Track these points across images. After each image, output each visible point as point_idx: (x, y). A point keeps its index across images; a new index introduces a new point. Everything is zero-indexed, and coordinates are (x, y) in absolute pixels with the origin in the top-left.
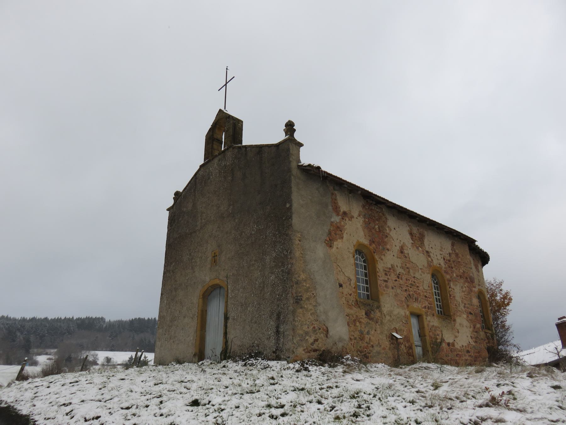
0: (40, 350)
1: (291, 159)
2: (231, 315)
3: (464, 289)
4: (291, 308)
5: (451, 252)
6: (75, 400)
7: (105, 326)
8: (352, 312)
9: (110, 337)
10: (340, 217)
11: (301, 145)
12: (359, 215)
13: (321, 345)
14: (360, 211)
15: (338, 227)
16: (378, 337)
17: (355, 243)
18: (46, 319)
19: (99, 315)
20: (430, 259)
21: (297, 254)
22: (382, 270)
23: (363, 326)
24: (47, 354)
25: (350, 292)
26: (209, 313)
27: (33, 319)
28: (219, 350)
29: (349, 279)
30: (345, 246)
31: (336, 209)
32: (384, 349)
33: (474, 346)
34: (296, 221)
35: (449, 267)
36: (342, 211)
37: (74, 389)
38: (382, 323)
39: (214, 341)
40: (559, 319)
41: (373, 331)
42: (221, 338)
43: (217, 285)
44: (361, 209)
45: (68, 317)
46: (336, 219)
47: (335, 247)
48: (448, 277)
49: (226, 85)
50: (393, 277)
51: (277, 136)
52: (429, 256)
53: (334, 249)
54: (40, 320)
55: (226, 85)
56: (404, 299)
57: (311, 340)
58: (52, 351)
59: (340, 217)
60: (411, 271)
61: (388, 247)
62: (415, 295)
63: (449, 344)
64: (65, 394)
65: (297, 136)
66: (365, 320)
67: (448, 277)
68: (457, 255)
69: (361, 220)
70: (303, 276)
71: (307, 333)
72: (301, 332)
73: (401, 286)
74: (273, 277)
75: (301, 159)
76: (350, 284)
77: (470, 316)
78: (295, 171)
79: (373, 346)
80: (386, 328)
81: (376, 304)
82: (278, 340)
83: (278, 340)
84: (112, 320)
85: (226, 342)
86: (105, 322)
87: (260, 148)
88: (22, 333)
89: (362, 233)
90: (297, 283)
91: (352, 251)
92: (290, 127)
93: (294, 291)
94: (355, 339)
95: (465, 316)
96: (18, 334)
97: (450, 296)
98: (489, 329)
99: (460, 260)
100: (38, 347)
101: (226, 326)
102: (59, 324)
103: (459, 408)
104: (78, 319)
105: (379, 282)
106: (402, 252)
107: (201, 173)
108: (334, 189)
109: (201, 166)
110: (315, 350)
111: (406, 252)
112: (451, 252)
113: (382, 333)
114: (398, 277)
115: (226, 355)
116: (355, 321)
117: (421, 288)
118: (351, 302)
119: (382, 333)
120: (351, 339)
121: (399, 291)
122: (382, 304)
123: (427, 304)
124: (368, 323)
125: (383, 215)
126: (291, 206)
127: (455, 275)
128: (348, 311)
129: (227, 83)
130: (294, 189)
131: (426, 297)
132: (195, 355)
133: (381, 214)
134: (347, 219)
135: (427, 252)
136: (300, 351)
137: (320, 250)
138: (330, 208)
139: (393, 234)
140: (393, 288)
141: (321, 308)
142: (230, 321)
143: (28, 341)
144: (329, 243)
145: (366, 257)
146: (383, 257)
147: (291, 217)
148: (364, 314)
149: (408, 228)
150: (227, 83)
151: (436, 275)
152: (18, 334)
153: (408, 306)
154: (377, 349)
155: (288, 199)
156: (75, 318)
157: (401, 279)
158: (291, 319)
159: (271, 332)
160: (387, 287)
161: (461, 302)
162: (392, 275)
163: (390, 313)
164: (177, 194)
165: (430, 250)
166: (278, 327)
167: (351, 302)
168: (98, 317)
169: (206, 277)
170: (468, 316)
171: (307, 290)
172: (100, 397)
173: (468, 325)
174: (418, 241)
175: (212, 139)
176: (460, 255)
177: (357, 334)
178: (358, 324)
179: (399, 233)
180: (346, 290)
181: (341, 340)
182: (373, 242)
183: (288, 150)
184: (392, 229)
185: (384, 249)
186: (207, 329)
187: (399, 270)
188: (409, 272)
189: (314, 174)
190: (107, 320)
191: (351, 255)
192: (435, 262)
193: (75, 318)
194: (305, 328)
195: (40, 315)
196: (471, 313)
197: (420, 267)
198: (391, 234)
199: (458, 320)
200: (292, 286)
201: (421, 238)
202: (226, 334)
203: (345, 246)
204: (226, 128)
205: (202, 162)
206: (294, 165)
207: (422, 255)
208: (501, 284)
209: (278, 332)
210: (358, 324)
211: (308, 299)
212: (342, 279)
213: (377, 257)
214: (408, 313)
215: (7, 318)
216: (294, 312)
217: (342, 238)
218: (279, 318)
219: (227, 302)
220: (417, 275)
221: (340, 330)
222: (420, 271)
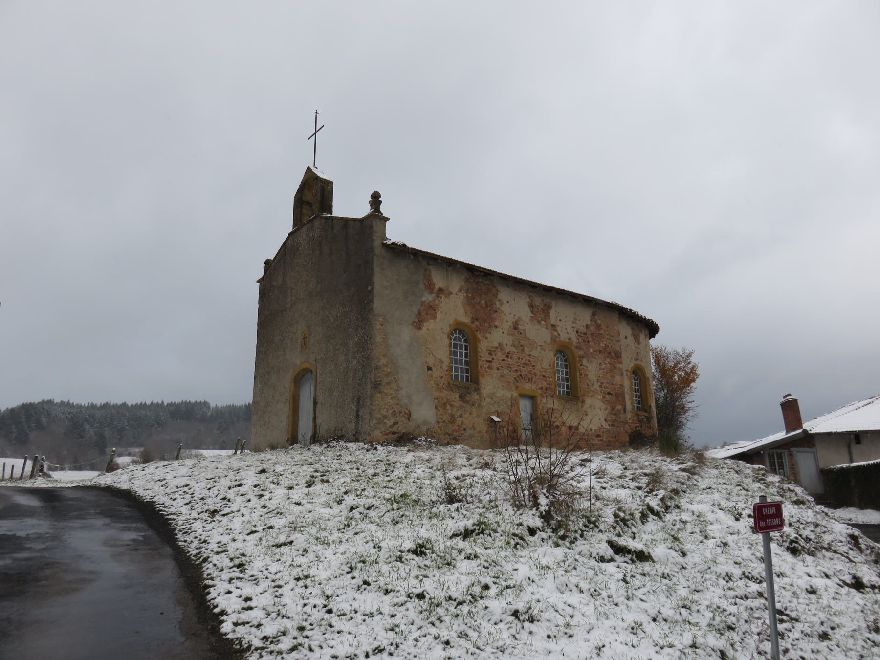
0: (120, 450)
1: (374, 237)
2: (319, 400)
3: (603, 366)
4: (369, 393)
5: (589, 323)
6: (168, 477)
7: (209, 413)
8: (443, 395)
9: (218, 429)
10: (434, 295)
11: (387, 219)
12: (460, 291)
13: (401, 428)
14: (461, 286)
15: (431, 307)
16: (473, 420)
17: (451, 322)
18: (124, 404)
19: (200, 398)
20: (556, 334)
21: (379, 339)
22: (484, 350)
23: (455, 409)
24: (129, 454)
25: (441, 375)
26: (301, 398)
27: (106, 406)
28: (310, 434)
29: (441, 362)
30: (438, 328)
31: (430, 287)
32: (480, 432)
33: (608, 431)
34: (378, 305)
35: (584, 341)
36: (437, 288)
37: (168, 470)
38: (479, 406)
39: (305, 427)
40: (785, 397)
41: (468, 414)
42: (311, 424)
43: (307, 368)
44: (463, 283)
45: (155, 402)
46: (428, 297)
47: (425, 328)
48: (581, 353)
49: (315, 134)
50: (500, 355)
51: (360, 210)
52: (556, 330)
53: (424, 331)
54: (115, 406)
55: (315, 134)
56: (512, 380)
57: (390, 423)
58: (137, 450)
59: (434, 295)
60: (526, 348)
61: (497, 323)
62: (529, 376)
63: (570, 428)
64: (160, 473)
65: (384, 209)
66: (458, 403)
67: (581, 353)
68: (598, 326)
69: (462, 295)
70: (383, 361)
71: (385, 417)
72: (379, 416)
73: (509, 367)
74: (355, 362)
75: (388, 235)
76: (441, 367)
77: (608, 397)
78: (378, 250)
79: (465, 429)
80: (485, 411)
81: (473, 386)
82: (357, 423)
83: (357, 423)
84: (219, 405)
85: (315, 427)
86: (209, 408)
87: (346, 221)
88: (92, 426)
89: (462, 311)
90: (376, 368)
91: (447, 331)
92: (376, 199)
93: (372, 377)
94: (444, 422)
95: (600, 397)
96: (87, 427)
97: (581, 374)
98: (646, 411)
99: (602, 332)
100: (116, 445)
101: (315, 410)
102: (143, 412)
103: (828, 549)
104: (171, 405)
105: (480, 363)
106: (515, 328)
107: (290, 242)
108: (429, 264)
109: (290, 234)
110: (394, 433)
111: (521, 327)
112: (589, 323)
113: (478, 416)
114: (507, 357)
115: (315, 439)
116: (445, 404)
117: (538, 367)
118: (441, 385)
119: (478, 416)
120: (438, 422)
121: (506, 372)
122: (482, 386)
123: (544, 384)
124: (461, 407)
125: (494, 287)
126: (372, 289)
127: (591, 350)
128: (437, 394)
129: (316, 132)
130: (377, 270)
131: (544, 376)
132: (288, 441)
133: (490, 286)
134: (443, 297)
135: (553, 326)
136: (377, 433)
137: (406, 333)
138: (422, 286)
139: (505, 308)
140: (498, 369)
141: (403, 392)
142: (318, 406)
143: (101, 436)
144: (418, 324)
145: (465, 337)
146: (488, 335)
147: (372, 301)
148: (457, 397)
149: (528, 300)
150: (316, 132)
151: (563, 351)
152: (87, 427)
153: (517, 387)
154: (469, 432)
155: (369, 281)
156: (165, 404)
157: (512, 358)
158: (368, 404)
159: (352, 417)
160: (490, 367)
161: (595, 381)
162: (499, 354)
163: (492, 396)
164: (268, 262)
165: (558, 323)
166: (358, 411)
167: (441, 385)
168: (198, 401)
169: (297, 360)
170: (604, 397)
171: (388, 375)
172: (190, 474)
173: (604, 406)
174: (541, 314)
175: (300, 201)
176: (603, 326)
177: (446, 418)
178: (448, 407)
179: (513, 307)
180: (436, 373)
181: (425, 423)
182: (477, 319)
183: (371, 227)
184: (505, 302)
185: (490, 326)
186: (300, 414)
187: (508, 349)
188: (523, 350)
189: (400, 251)
190: (55, 402)
191: (445, 336)
192: (563, 337)
193: (165, 404)
194: (384, 412)
195: (116, 399)
196: (609, 393)
197: (539, 344)
198: (502, 308)
199: (588, 401)
200: (370, 372)
201: (547, 309)
202: (315, 418)
203: (438, 328)
204: (314, 194)
205: (291, 229)
206: (377, 243)
207: (544, 329)
208: (689, 356)
209: (357, 416)
210: (448, 407)
211: (388, 384)
212: (431, 361)
213: (479, 336)
214: (515, 395)
215: (69, 405)
216: (371, 397)
217: (435, 318)
218: (359, 401)
219: (316, 387)
220: (535, 353)
221: (425, 413)
222: (539, 349)
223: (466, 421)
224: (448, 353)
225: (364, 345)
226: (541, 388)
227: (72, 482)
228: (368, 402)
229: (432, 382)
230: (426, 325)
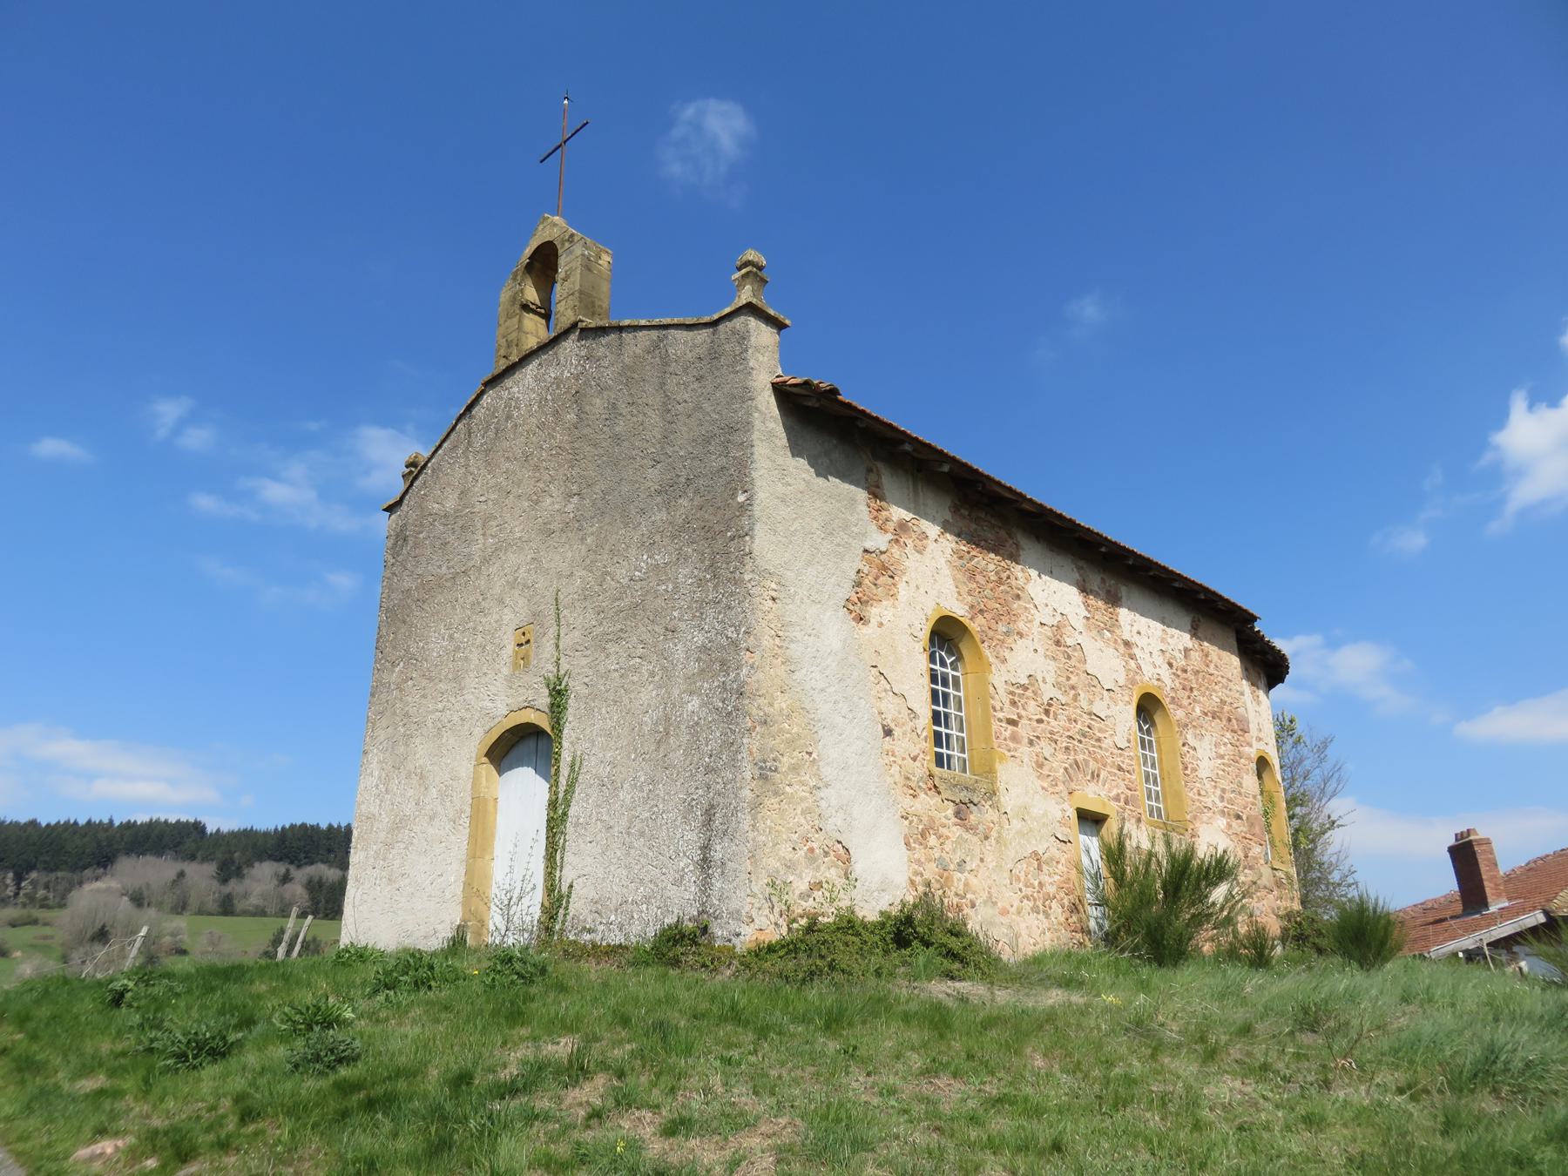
4: (746, 793)
34: (764, 544)
61: (1021, 625)
70: (782, 703)
71: (790, 866)
74: (694, 704)
82: (705, 886)
135: (1127, 644)
137: (834, 629)
141: (830, 797)
144: (857, 608)
156: (117, 823)
166: (705, 848)
170: (1229, 825)
187: (1048, 692)
193: (117, 823)
194: (785, 850)
196: (1238, 817)
209: (705, 863)
216: (756, 806)
218: (711, 819)
223: (974, 881)
224: (928, 696)
225: (722, 660)
226: (1117, 798)
227: (1010, 489)
228: (746, 821)
229: (895, 769)
230: (874, 612)
